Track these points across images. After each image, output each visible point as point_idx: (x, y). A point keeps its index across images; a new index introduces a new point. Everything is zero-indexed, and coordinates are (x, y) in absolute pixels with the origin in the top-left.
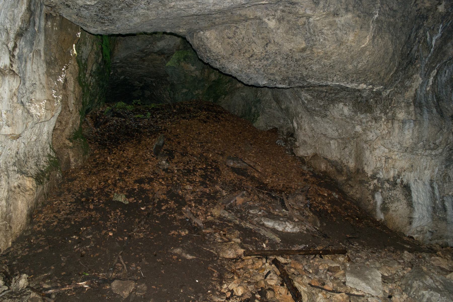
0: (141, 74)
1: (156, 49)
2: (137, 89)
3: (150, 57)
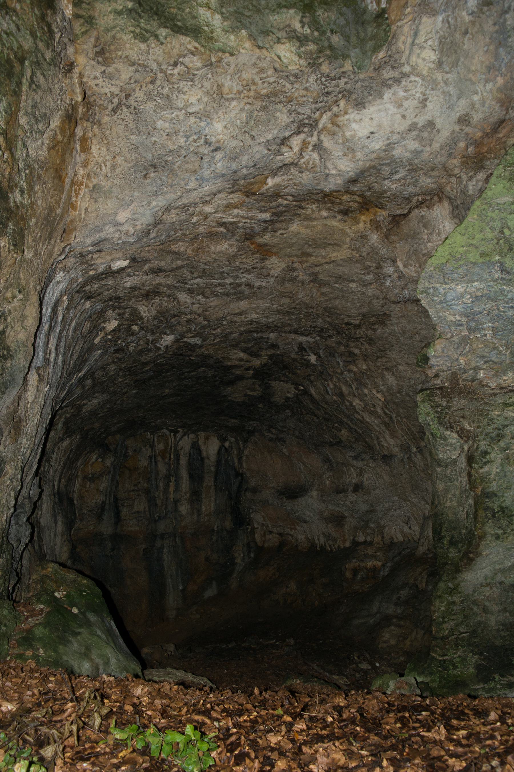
0: (252, 322)
1: (341, 166)
2: (241, 378)
3: (295, 227)
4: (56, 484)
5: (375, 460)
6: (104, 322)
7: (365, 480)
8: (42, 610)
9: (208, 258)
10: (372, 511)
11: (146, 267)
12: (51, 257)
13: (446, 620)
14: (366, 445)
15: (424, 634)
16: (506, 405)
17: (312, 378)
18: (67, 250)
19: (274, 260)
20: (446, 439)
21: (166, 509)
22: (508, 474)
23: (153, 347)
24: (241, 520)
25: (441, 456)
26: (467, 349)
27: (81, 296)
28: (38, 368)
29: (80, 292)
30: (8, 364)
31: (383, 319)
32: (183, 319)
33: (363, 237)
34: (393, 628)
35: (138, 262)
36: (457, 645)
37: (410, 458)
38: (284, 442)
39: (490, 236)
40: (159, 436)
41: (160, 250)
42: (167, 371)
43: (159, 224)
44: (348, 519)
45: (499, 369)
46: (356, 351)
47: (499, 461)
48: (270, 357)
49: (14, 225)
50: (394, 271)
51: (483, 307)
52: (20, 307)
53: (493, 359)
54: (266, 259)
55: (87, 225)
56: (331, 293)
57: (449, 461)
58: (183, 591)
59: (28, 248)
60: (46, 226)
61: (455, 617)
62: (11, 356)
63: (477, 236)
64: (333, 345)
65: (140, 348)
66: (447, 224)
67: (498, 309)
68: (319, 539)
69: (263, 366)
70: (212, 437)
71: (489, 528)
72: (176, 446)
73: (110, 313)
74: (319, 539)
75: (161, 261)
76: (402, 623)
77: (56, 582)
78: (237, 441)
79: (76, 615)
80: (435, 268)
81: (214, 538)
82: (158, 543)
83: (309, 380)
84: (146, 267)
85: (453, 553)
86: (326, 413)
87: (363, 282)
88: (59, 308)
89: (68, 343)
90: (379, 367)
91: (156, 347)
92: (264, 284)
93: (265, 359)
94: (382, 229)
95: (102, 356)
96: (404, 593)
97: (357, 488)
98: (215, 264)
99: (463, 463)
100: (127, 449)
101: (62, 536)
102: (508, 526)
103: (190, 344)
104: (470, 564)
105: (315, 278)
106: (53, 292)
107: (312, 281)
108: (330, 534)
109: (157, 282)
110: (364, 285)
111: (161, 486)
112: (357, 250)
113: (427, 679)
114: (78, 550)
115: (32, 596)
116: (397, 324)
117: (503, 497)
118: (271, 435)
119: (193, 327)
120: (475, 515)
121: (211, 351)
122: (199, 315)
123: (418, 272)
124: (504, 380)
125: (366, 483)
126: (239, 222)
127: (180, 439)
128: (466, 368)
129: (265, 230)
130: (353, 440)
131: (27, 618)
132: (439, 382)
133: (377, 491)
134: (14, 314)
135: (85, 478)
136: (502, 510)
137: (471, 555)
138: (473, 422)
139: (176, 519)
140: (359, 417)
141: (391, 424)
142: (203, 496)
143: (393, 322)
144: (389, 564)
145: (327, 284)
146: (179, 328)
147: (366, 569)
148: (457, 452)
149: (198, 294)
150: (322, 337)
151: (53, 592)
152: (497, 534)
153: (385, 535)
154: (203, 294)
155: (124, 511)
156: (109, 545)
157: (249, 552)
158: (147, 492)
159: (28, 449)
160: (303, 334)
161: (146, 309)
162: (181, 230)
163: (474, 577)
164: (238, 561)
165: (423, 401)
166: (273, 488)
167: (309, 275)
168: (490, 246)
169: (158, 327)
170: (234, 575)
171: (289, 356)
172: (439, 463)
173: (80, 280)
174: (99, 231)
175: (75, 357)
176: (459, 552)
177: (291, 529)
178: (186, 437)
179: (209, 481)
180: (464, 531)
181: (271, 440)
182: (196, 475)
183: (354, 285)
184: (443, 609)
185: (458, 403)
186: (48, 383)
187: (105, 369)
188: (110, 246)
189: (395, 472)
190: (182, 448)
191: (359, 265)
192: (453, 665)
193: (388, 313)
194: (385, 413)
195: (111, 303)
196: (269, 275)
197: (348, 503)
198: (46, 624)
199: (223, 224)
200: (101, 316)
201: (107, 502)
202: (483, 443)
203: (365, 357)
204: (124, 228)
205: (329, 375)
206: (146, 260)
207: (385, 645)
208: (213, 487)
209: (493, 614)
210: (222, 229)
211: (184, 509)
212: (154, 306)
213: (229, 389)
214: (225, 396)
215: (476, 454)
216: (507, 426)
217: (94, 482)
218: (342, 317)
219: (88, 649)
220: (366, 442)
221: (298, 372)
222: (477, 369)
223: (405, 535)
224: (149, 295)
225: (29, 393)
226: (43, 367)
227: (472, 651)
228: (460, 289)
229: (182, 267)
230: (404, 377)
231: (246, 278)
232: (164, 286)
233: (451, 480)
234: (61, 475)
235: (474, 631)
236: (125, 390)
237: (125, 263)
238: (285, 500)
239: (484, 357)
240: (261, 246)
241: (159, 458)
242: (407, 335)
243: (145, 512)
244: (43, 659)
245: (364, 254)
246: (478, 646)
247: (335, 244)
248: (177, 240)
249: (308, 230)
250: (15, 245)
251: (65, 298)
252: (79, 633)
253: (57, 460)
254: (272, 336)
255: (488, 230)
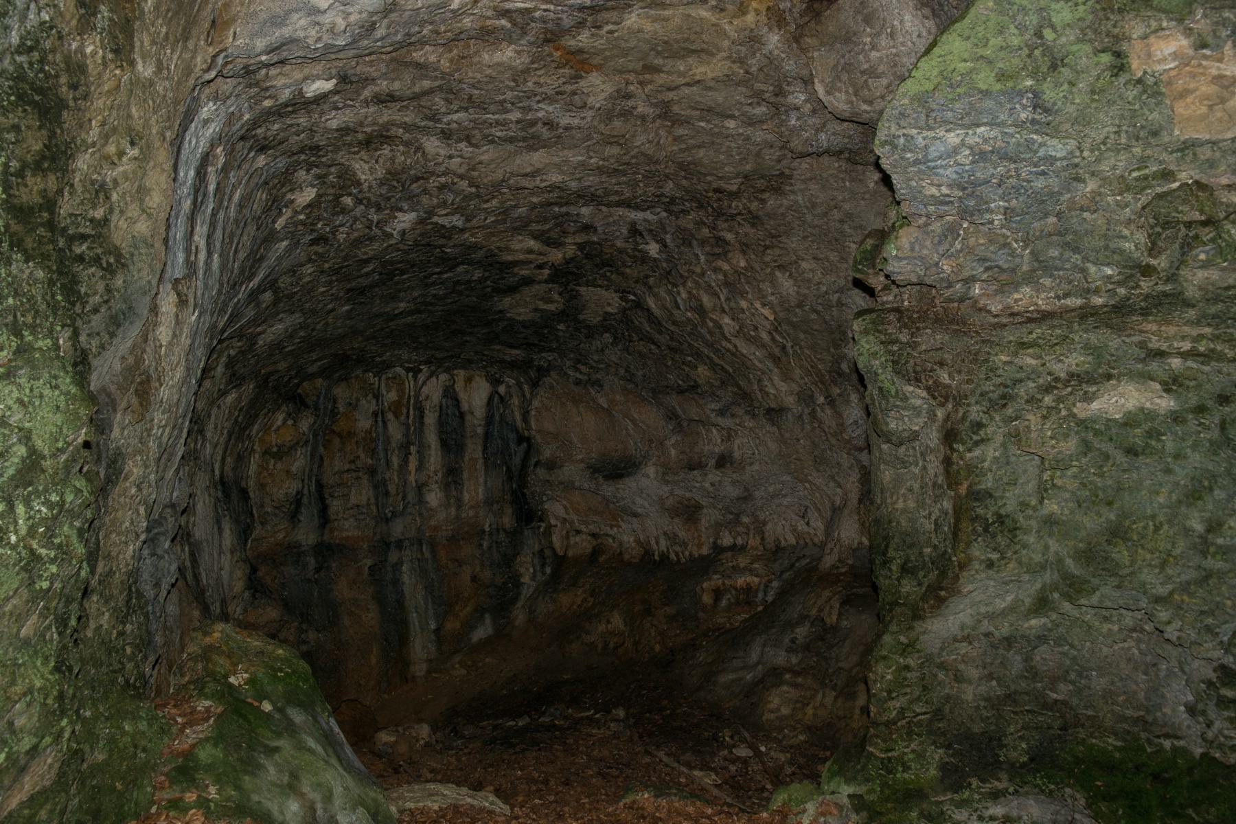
0: (552, 188)
2: (528, 281)
4: (217, 466)
5: (754, 416)
6: (292, 190)
7: (736, 447)
8: (208, 709)
9: (479, 76)
10: (746, 498)
11: (367, 93)
12: (189, 75)
13: (894, 695)
14: (742, 395)
15: (836, 698)
16: (1023, 345)
17: (651, 281)
18: (220, 61)
19: (594, 78)
20: (905, 398)
21: (404, 498)
22: (1013, 459)
23: (379, 233)
24: (528, 514)
25: (893, 426)
26: (958, 246)
27: (248, 145)
28: (176, 282)
29: (246, 139)
30: (119, 282)
31: (778, 183)
32: (433, 183)
33: (753, 40)
34: (785, 688)
35: (352, 83)
36: (910, 733)
37: (813, 414)
38: (601, 386)
39: (1016, 41)
40: (388, 379)
41: (392, 60)
42: (403, 273)
43: (391, 11)
44: (705, 511)
45: (1007, 281)
46: (729, 236)
47: (999, 439)
48: (581, 247)
49: (111, 10)
50: (806, 101)
51: (992, 171)
52: (134, 172)
53: (1001, 263)
54: (581, 77)
55: (255, 13)
56: (692, 138)
57: (906, 434)
58: (437, 631)
59: (144, 58)
60: (176, 13)
61: (908, 690)
62: (124, 265)
63: (992, 42)
64: (691, 226)
65: (356, 235)
66: (907, 17)
67: (1019, 175)
68: (657, 543)
69: (568, 262)
70: (477, 379)
71: (978, 551)
72: (417, 395)
73: (302, 174)
74: (657, 543)
75: (393, 80)
76: (800, 680)
77: (229, 657)
78: (519, 384)
79: (268, 715)
80: (912, 99)
81: (485, 544)
82: (393, 556)
83: (645, 284)
84: (367, 93)
85: (908, 587)
86: (672, 339)
87: (750, 118)
88: (210, 169)
89: (228, 231)
90: (767, 265)
91: (384, 233)
92: (576, 122)
93: (571, 251)
94: (787, 24)
95: (288, 250)
96: (802, 632)
97: (723, 461)
98: (491, 86)
99: (933, 438)
100: (335, 402)
101: (232, 553)
102: (1008, 546)
103: (443, 226)
104: (939, 607)
105: (665, 112)
106: (198, 140)
107: (659, 116)
108: (675, 535)
109: (386, 118)
110: (750, 125)
111: (395, 461)
112: (741, 61)
113: (861, 790)
114: (260, 574)
115: (189, 682)
116: (802, 191)
117: (1002, 498)
118: (578, 375)
119: (450, 198)
120: (956, 532)
121: (480, 238)
122: (461, 177)
123: (851, 102)
124: (1016, 301)
125: (737, 454)
126: (535, 9)
127: (424, 383)
128: (953, 278)
129: (581, 24)
130: (717, 383)
131: (182, 731)
132: (891, 298)
133: (756, 467)
134: (126, 186)
135: (266, 453)
136: (1001, 519)
137: (943, 593)
138: (959, 372)
139: (421, 514)
140: (729, 346)
141: (784, 359)
142: (465, 475)
143: (796, 188)
144: (775, 584)
145: (687, 121)
146: (425, 199)
147: (736, 589)
148: (921, 421)
149: (460, 140)
150: (670, 212)
151: (226, 676)
152: (989, 559)
153: (767, 534)
154: (468, 139)
155: (335, 505)
156: (312, 562)
157: (543, 566)
158: (372, 472)
159: (165, 426)
160: (637, 207)
161: (366, 167)
162: (431, 23)
163: (941, 627)
164: (526, 579)
165: (866, 332)
166: (582, 461)
167: (656, 105)
168: (1016, 61)
169: (389, 199)
170: (520, 604)
171: (613, 245)
172: (887, 437)
173: (247, 116)
174: (281, 25)
175: (242, 255)
176: (920, 585)
177: (612, 527)
178: (434, 379)
179: (474, 450)
180: (928, 550)
181: (578, 383)
182: (452, 443)
183: (731, 124)
184: (889, 677)
185: (930, 338)
186: (196, 306)
187: (295, 272)
188: (301, 53)
189: (787, 435)
190: (427, 397)
191: (744, 90)
192: (904, 765)
193: (787, 171)
194: (773, 339)
195: (303, 157)
196: (584, 106)
197: (707, 485)
198: (218, 739)
199: (506, 13)
200: (286, 179)
201: (306, 492)
202: (975, 408)
203: (745, 248)
204: (327, 19)
205: (682, 276)
206: (367, 79)
207: (772, 716)
208: (481, 461)
209: (970, 683)
210: (503, 22)
211: (434, 497)
212: (381, 161)
213: (507, 301)
214: (501, 312)
215: (962, 427)
216: (1021, 381)
217: (281, 459)
218: (709, 178)
219: (294, 776)
220: (739, 387)
221: (628, 270)
222: (970, 281)
223: (799, 536)
224: (373, 141)
225: (162, 329)
226: (184, 278)
227: (934, 743)
228: (953, 138)
229: (431, 91)
230: (809, 281)
231: (544, 110)
232: (399, 126)
233: (904, 464)
234: (225, 452)
235: (939, 710)
236: (330, 307)
237: (329, 85)
238: (601, 480)
239: (985, 260)
240: (573, 53)
241: (390, 416)
242: (819, 210)
243: (369, 505)
244: (216, 805)
245: (754, 69)
246: (944, 734)
247: (702, 50)
248: (423, 43)
249: (657, 26)
250: (116, 51)
251: (219, 150)
252: (276, 750)
253: (216, 431)
254: (585, 211)
255: (1013, 30)
